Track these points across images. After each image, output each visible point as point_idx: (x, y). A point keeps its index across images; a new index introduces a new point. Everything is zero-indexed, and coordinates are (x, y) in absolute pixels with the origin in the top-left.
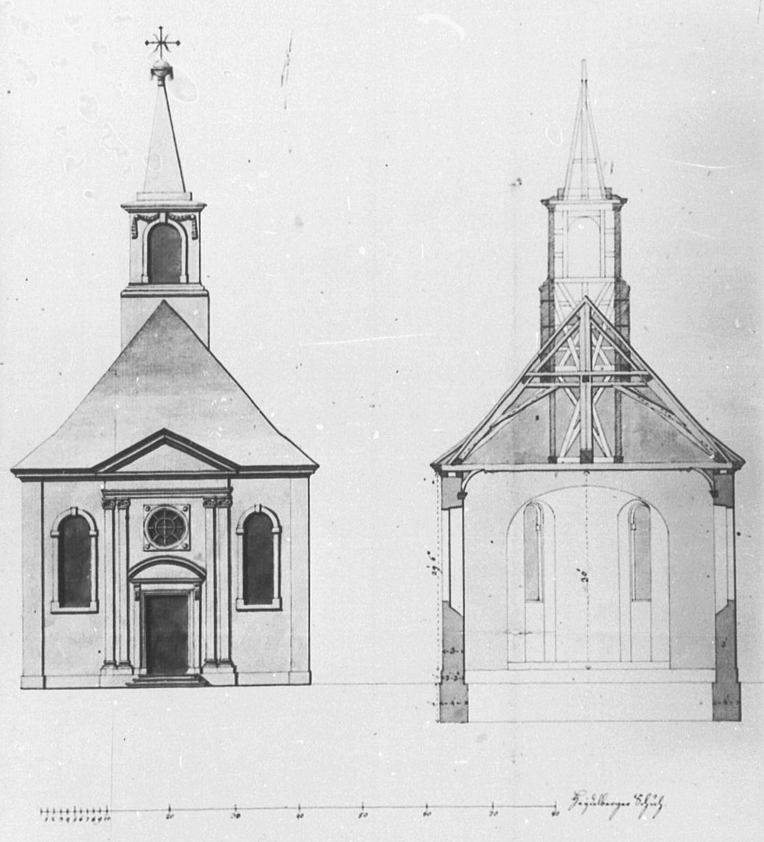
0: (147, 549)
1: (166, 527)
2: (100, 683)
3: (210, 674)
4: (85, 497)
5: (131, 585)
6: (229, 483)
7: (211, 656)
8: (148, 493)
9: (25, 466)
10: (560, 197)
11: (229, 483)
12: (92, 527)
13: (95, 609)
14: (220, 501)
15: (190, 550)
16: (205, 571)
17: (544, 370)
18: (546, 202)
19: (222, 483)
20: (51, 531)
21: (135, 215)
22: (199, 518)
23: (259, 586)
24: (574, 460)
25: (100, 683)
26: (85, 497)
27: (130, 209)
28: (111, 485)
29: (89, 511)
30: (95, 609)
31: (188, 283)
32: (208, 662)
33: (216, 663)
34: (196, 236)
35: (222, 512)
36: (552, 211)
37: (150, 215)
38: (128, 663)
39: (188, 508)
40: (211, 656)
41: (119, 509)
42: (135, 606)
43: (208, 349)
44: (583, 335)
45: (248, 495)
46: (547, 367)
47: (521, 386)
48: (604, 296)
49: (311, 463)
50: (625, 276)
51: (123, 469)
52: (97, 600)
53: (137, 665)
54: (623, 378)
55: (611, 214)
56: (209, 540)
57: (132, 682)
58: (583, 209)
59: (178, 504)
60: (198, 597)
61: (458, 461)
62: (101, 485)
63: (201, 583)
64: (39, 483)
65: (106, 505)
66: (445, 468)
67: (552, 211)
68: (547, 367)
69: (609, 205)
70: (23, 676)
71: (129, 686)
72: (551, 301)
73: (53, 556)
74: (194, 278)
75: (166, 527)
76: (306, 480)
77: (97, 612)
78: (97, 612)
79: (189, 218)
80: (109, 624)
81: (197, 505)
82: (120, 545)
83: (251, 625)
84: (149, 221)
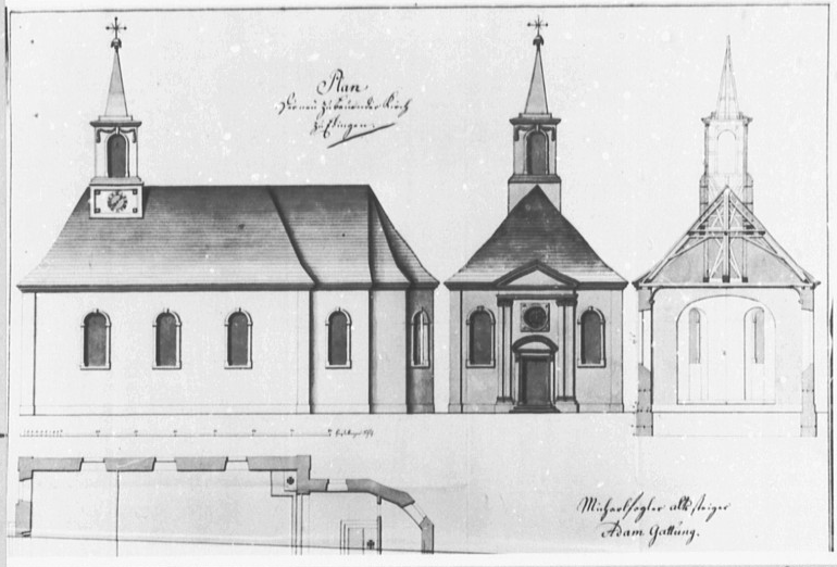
0: (523, 330)
1: (536, 319)
3: (558, 405)
4: (489, 299)
6: (574, 292)
7: (561, 394)
9: (23, 284)
10: (713, 115)
11: (574, 292)
14: (564, 302)
17: (698, 231)
18: (749, 120)
19: (571, 292)
21: (98, 128)
22: (556, 312)
24: (719, 281)
26: (489, 299)
27: (94, 124)
28: (503, 293)
32: (559, 398)
33: (565, 398)
34: (135, 140)
35: (570, 309)
36: (707, 125)
37: (111, 129)
38: (510, 399)
39: (548, 306)
40: (561, 394)
42: (516, 366)
44: (725, 209)
45: (586, 299)
46: (702, 227)
47: (687, 237)
48: (736, 184)
49: (621, 280)
50: (749, 171)
51: (559, 283)
52: (180, 362)
53: (517, 399)
54: (748, 233)
55: (742, 128)
58: (725, 125)
59: (543, 303)
61: (648, 281)
62: (496, 292)
64: (307, 293)
65: (499, 304)
66: (641, 284)
67: (707, 125)
68: (702, 227)
69: (741, 123)
71: (511, 412)
72: (706, 187)
74: (133, 173)
75: (536, 319)
77: (350, 368)
78: (350, 368)
79: (130, 131)
81: (553, 303)
82: (510, 328)
83: (587, 376)
84: (108, 132)
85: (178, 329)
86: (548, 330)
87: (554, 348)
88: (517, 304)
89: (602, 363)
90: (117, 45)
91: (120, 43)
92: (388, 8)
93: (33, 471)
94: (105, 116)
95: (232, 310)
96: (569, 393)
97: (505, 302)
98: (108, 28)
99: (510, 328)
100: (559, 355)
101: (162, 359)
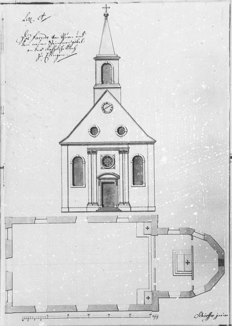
1: (107, 162)
2: (148, 209)
4: (82, 151)
5: (98, 180)
8: (101, 149)
12: (84, 161)
13: (85, 187)
15: (115, 168)
16: (119, 176)
20: (71, 162)
23: (137, 178)
25: (148, 209)
29: (84, 157)
30: (85, 187)
31: (114, 83)
40: (122, 201)
41: (93, 154)
43: (121, 105)
45: (134, 151)
56: (122, 167)
57: (98, 210)
60: (117, 184)
63: (117, 179)
65: (89, 153)
70: (62, 208)
73: (81, 316)
74: (116, 82)
75: (107, 162)
76: (153, 145)
77: (85, 187)
80: (85, 195)
82: (93, 168)
85: (144, 163)
86: (114, 168)
87: (118, 177)
88: (99, 153)
89: (84, 186)
90: (106, 16)
91: (108, 15)
92: (88, 3)
93: (12, 224)
94: (99, 55)
95: (75, 155)
96: (127, 201)
97: (91, 152)
98: (103, 8)
99: (93, 168)
100: (120, 181)
101: (135, 183)
